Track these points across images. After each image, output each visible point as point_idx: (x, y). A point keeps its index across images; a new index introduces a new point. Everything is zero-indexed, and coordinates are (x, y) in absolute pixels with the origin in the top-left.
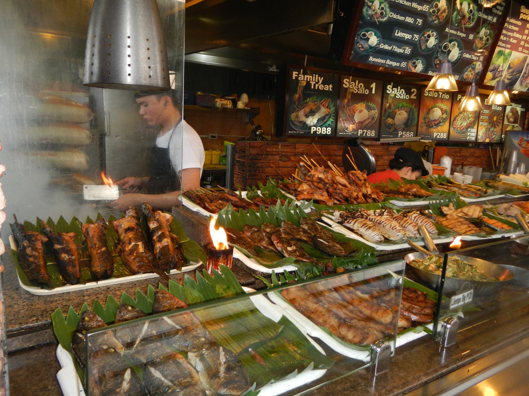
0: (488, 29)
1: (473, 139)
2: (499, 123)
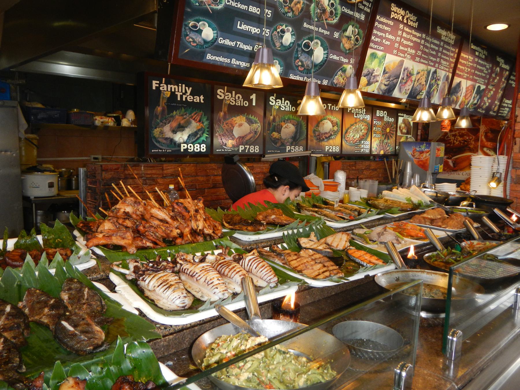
0: (356, 27)
1: (367, 151)
2: (393, 134)
